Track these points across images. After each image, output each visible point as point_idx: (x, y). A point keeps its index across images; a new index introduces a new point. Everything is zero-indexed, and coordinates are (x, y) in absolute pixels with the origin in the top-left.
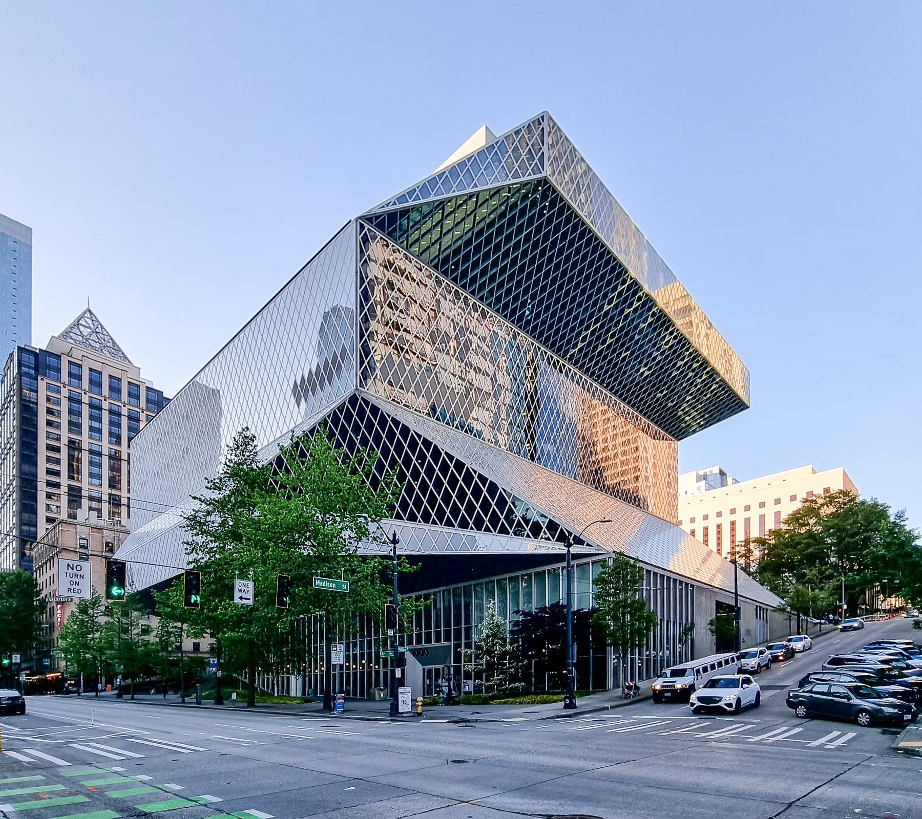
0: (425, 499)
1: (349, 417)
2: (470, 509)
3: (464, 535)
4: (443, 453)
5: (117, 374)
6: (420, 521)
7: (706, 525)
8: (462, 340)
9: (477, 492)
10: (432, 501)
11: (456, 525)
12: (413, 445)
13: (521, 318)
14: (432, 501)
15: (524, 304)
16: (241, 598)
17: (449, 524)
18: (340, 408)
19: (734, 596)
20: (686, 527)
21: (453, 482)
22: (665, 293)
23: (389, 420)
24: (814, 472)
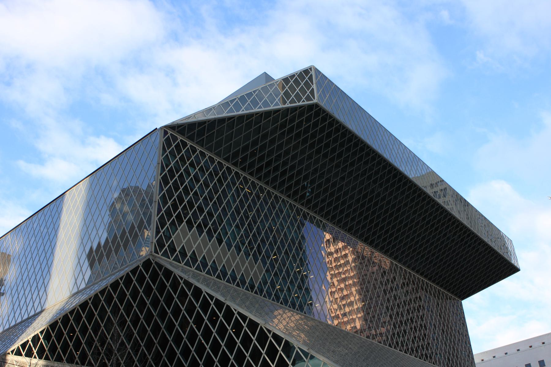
0: (90, 326)
1: (141, 279)
8: (251, 215)
10: (78, 344)
12: (205, 305)
13: (303, 197)
14: (78, 344)
15: (304, 188)
18: (134, 271)
21: (247, 341)
22: (416, 173)
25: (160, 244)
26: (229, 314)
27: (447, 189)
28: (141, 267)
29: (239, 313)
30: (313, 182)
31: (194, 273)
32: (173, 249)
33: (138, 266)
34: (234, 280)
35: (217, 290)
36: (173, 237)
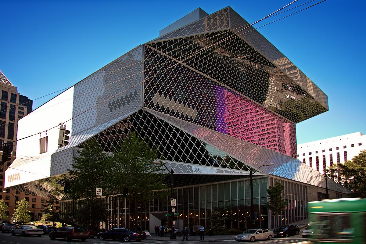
1: (138, 118)
2: (180, 152)
3: (224, 170)
4: (185, 134)
6: (224, 170)
7: (317, 154)
11: (192, 162)
16: (98, 194)
17: (188, 162)
19: (326, 190)
20: (300, 158)
23: (158, 120)
24: (362, 135)
25: (146, 102)
26: (182, 134)
28: (137, 113)
29: (187, 134)
31: (168, 117)
32: (153, 105)
33: (136, 112)
34: (173, 114)
35: (174, 121)
36: (152, 99)
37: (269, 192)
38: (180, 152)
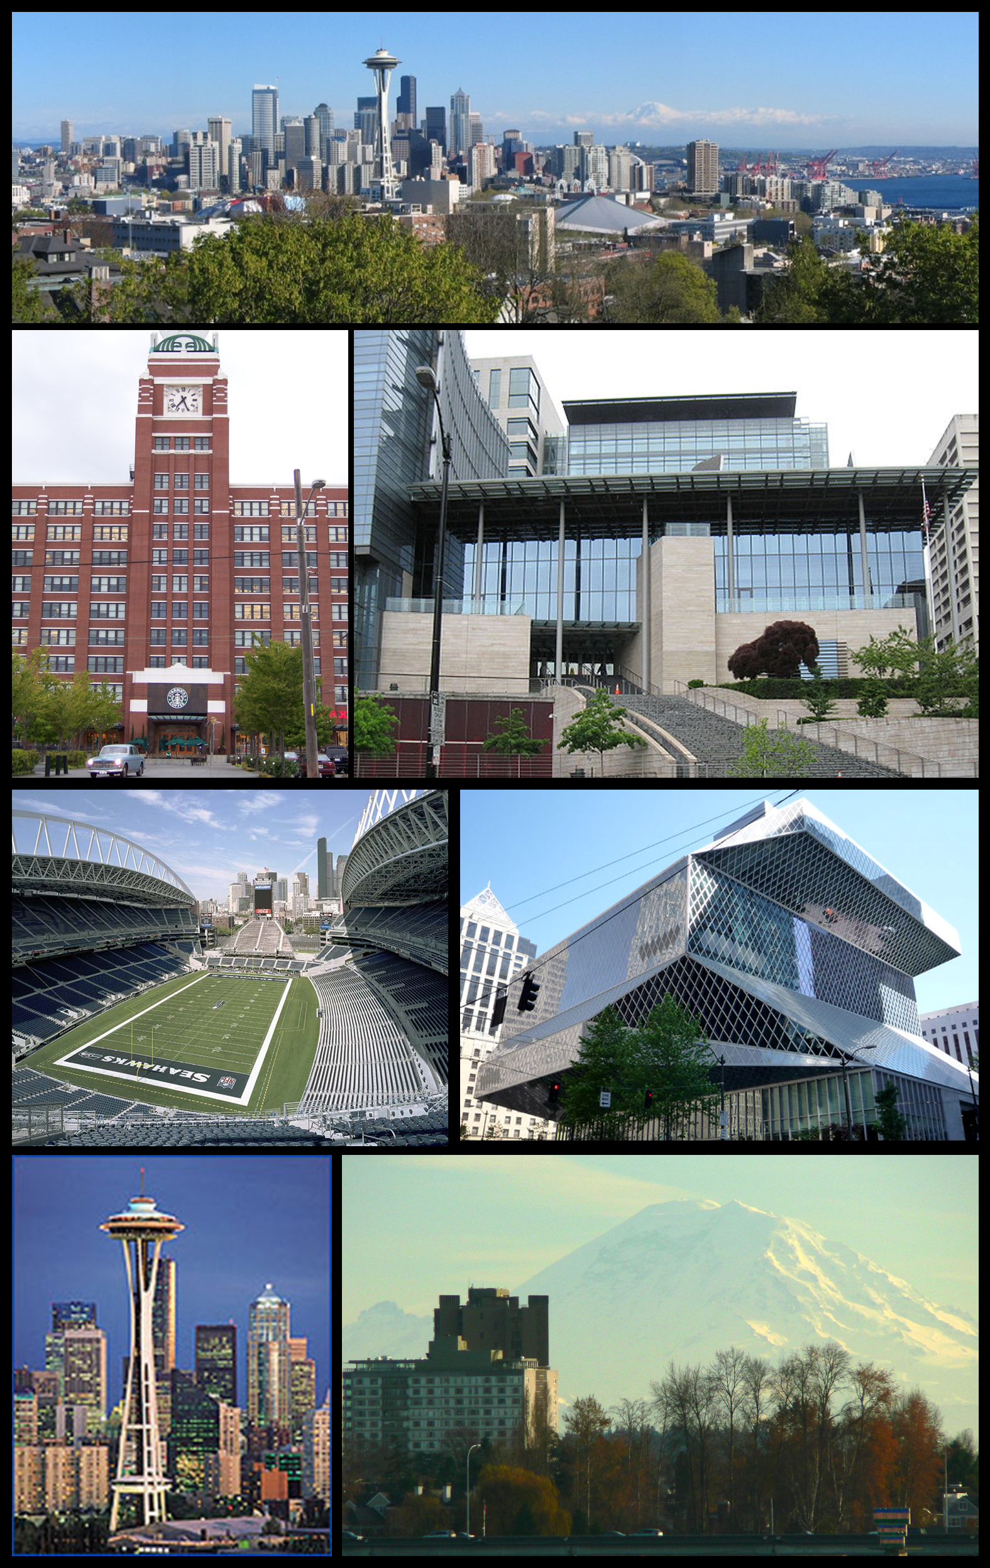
1: (680, 970)
2: (729, 1029)
5: (500, 929)
9: (710, 983)
10: (739, 1027)
12: (725, 989)
14: (739, 1027)
15: (795, 897)
21: (694, 977)
25: (692, 945)
27: (901, 890)
30: (802, 892)
32: (701, 949)
37: (878, 1100)
38: (729, 1029)
